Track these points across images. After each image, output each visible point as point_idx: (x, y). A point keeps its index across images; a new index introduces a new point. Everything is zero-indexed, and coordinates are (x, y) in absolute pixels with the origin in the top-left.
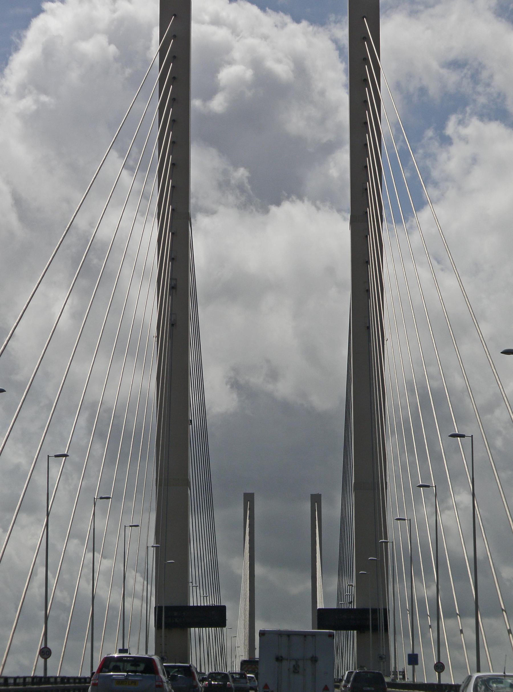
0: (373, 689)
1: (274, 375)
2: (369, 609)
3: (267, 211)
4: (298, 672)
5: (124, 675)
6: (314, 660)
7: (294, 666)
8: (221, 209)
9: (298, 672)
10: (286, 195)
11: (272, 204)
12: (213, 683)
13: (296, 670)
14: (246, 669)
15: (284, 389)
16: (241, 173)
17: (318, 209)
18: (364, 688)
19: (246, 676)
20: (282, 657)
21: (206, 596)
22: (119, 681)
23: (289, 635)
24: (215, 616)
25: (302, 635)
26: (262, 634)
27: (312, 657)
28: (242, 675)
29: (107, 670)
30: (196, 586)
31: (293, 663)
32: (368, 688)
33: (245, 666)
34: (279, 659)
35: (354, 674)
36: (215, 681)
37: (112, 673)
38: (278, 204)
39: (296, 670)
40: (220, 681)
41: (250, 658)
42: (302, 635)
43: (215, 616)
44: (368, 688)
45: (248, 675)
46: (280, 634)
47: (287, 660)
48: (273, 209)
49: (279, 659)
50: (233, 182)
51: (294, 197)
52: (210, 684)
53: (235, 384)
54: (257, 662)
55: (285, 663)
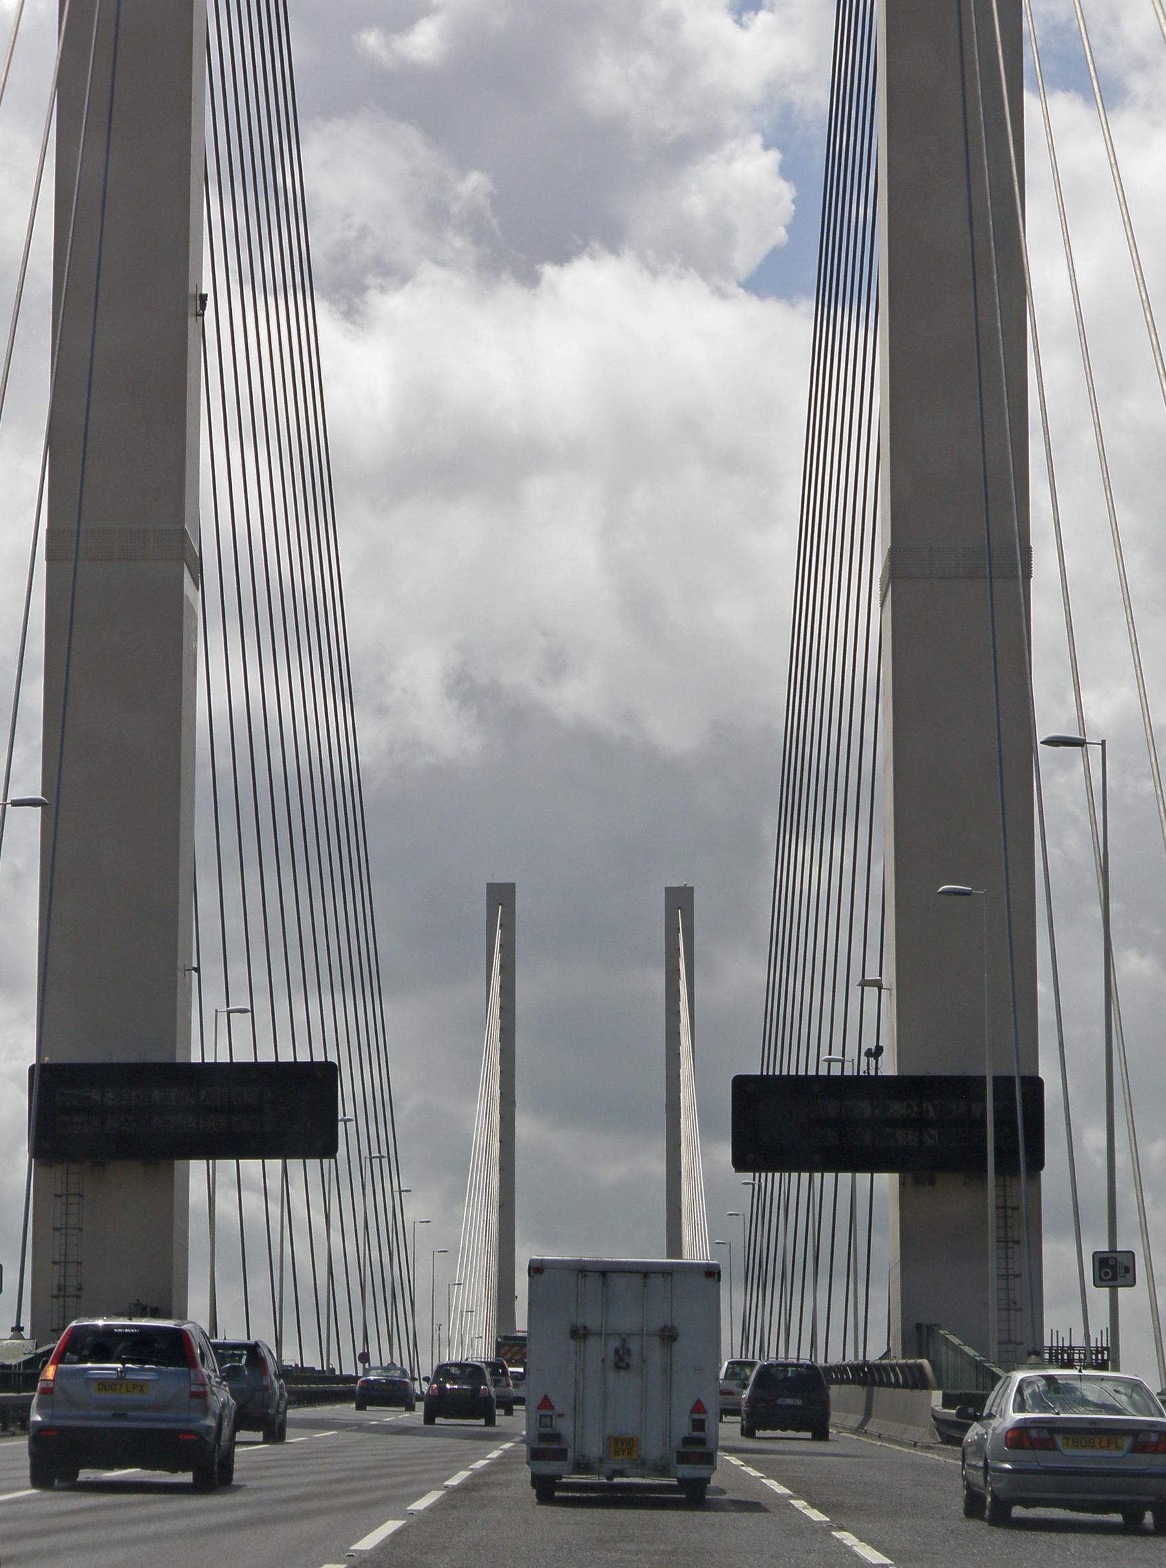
0: (799, 1402)
1: (557, 665)
2: (984, 1078)
3: (531, 280)
4: (627, 1366)
5: (115, 1369)
6: (669, 1336)
7: (617, 1351)
8: (429, 272)
9: (627, 1366)
10: (580, 242)
11: (542, 262)
12: (448, 1386)
13: (621, 1361)
14: (508, 1356)
15: (577, 698)
16: (474, 184)
17: (654, 273)
18: (780, 1401)
19: (505, 1371)
20: (585, 1328)
21: (381, 1158)
22: (104, 1384)
23: (605, 1272)
24: (287, 1110)
25: (637, 1272)
26: (536, 1269)
27: (663, 1329)
28: (496, 1368)
29: (75, 1358)
30: (345, 1121)
31: (615, 1343)
32: (789, 1401)
33: (506, 1348)
34: (579, 1334)
35: (758, 1367)
36: (455, 1383)
37: (89, 1365)
38: (562, 258)
39: (621, 1361)
40: (464, 1383)
41: (172, 1167)
42: (637, 1272)
43: (287, 1110)
44: (789, 1401)
45: (510, 1369)
46: (581, 1270)
47: (600, 1335)
48: (549, 271)
49: (579, 1334)
50: (455, 209)
51: (596, 245)
52: (442, 1389)
53: (468, 690)
54: (523, 1338)
55: (594, 1343)
